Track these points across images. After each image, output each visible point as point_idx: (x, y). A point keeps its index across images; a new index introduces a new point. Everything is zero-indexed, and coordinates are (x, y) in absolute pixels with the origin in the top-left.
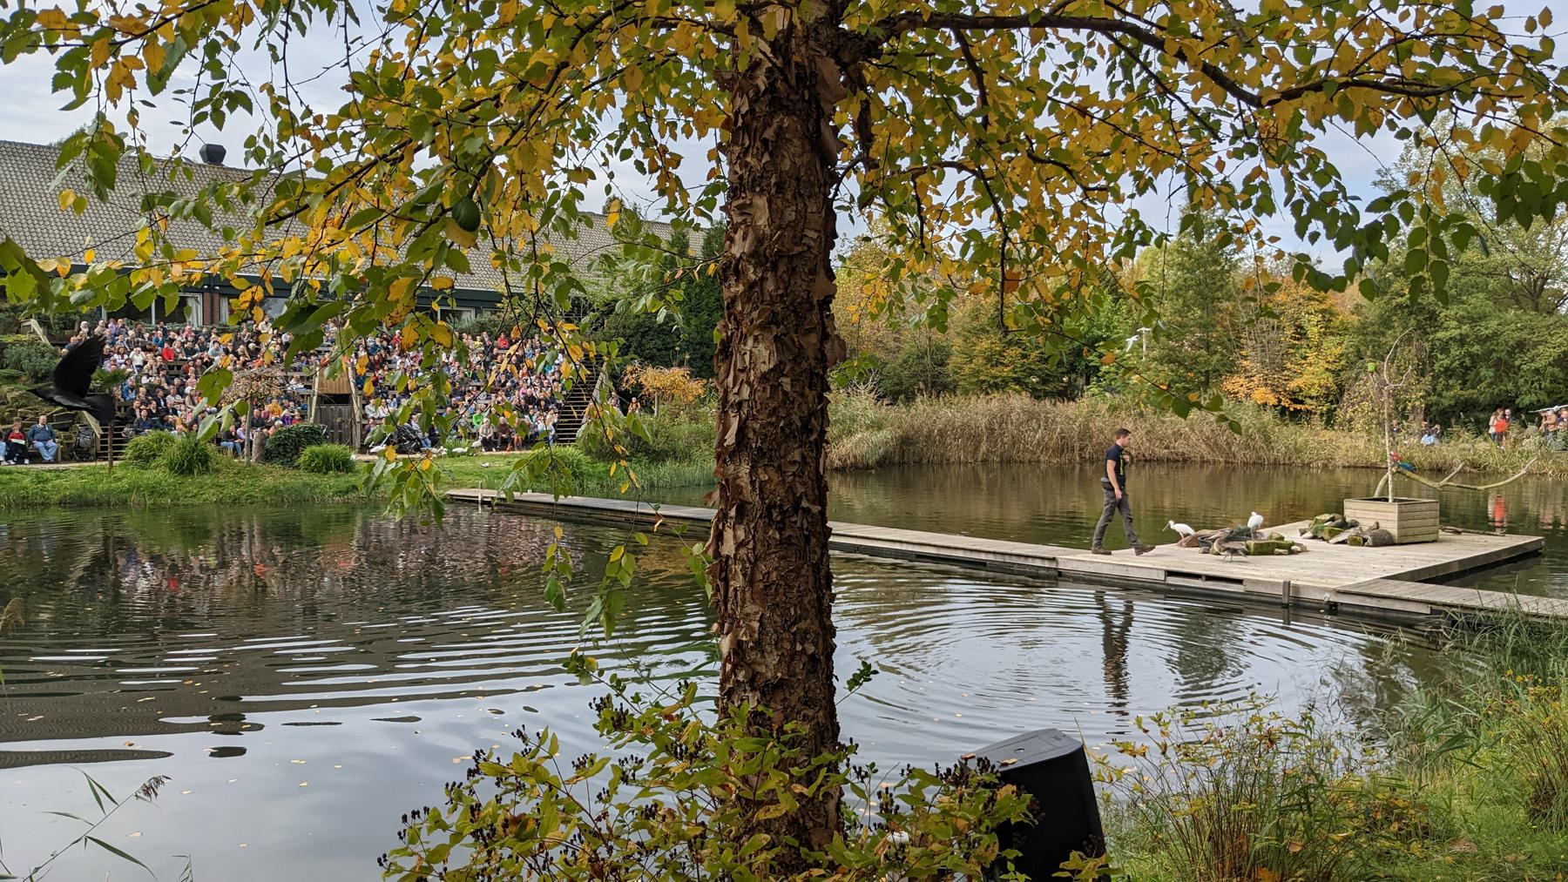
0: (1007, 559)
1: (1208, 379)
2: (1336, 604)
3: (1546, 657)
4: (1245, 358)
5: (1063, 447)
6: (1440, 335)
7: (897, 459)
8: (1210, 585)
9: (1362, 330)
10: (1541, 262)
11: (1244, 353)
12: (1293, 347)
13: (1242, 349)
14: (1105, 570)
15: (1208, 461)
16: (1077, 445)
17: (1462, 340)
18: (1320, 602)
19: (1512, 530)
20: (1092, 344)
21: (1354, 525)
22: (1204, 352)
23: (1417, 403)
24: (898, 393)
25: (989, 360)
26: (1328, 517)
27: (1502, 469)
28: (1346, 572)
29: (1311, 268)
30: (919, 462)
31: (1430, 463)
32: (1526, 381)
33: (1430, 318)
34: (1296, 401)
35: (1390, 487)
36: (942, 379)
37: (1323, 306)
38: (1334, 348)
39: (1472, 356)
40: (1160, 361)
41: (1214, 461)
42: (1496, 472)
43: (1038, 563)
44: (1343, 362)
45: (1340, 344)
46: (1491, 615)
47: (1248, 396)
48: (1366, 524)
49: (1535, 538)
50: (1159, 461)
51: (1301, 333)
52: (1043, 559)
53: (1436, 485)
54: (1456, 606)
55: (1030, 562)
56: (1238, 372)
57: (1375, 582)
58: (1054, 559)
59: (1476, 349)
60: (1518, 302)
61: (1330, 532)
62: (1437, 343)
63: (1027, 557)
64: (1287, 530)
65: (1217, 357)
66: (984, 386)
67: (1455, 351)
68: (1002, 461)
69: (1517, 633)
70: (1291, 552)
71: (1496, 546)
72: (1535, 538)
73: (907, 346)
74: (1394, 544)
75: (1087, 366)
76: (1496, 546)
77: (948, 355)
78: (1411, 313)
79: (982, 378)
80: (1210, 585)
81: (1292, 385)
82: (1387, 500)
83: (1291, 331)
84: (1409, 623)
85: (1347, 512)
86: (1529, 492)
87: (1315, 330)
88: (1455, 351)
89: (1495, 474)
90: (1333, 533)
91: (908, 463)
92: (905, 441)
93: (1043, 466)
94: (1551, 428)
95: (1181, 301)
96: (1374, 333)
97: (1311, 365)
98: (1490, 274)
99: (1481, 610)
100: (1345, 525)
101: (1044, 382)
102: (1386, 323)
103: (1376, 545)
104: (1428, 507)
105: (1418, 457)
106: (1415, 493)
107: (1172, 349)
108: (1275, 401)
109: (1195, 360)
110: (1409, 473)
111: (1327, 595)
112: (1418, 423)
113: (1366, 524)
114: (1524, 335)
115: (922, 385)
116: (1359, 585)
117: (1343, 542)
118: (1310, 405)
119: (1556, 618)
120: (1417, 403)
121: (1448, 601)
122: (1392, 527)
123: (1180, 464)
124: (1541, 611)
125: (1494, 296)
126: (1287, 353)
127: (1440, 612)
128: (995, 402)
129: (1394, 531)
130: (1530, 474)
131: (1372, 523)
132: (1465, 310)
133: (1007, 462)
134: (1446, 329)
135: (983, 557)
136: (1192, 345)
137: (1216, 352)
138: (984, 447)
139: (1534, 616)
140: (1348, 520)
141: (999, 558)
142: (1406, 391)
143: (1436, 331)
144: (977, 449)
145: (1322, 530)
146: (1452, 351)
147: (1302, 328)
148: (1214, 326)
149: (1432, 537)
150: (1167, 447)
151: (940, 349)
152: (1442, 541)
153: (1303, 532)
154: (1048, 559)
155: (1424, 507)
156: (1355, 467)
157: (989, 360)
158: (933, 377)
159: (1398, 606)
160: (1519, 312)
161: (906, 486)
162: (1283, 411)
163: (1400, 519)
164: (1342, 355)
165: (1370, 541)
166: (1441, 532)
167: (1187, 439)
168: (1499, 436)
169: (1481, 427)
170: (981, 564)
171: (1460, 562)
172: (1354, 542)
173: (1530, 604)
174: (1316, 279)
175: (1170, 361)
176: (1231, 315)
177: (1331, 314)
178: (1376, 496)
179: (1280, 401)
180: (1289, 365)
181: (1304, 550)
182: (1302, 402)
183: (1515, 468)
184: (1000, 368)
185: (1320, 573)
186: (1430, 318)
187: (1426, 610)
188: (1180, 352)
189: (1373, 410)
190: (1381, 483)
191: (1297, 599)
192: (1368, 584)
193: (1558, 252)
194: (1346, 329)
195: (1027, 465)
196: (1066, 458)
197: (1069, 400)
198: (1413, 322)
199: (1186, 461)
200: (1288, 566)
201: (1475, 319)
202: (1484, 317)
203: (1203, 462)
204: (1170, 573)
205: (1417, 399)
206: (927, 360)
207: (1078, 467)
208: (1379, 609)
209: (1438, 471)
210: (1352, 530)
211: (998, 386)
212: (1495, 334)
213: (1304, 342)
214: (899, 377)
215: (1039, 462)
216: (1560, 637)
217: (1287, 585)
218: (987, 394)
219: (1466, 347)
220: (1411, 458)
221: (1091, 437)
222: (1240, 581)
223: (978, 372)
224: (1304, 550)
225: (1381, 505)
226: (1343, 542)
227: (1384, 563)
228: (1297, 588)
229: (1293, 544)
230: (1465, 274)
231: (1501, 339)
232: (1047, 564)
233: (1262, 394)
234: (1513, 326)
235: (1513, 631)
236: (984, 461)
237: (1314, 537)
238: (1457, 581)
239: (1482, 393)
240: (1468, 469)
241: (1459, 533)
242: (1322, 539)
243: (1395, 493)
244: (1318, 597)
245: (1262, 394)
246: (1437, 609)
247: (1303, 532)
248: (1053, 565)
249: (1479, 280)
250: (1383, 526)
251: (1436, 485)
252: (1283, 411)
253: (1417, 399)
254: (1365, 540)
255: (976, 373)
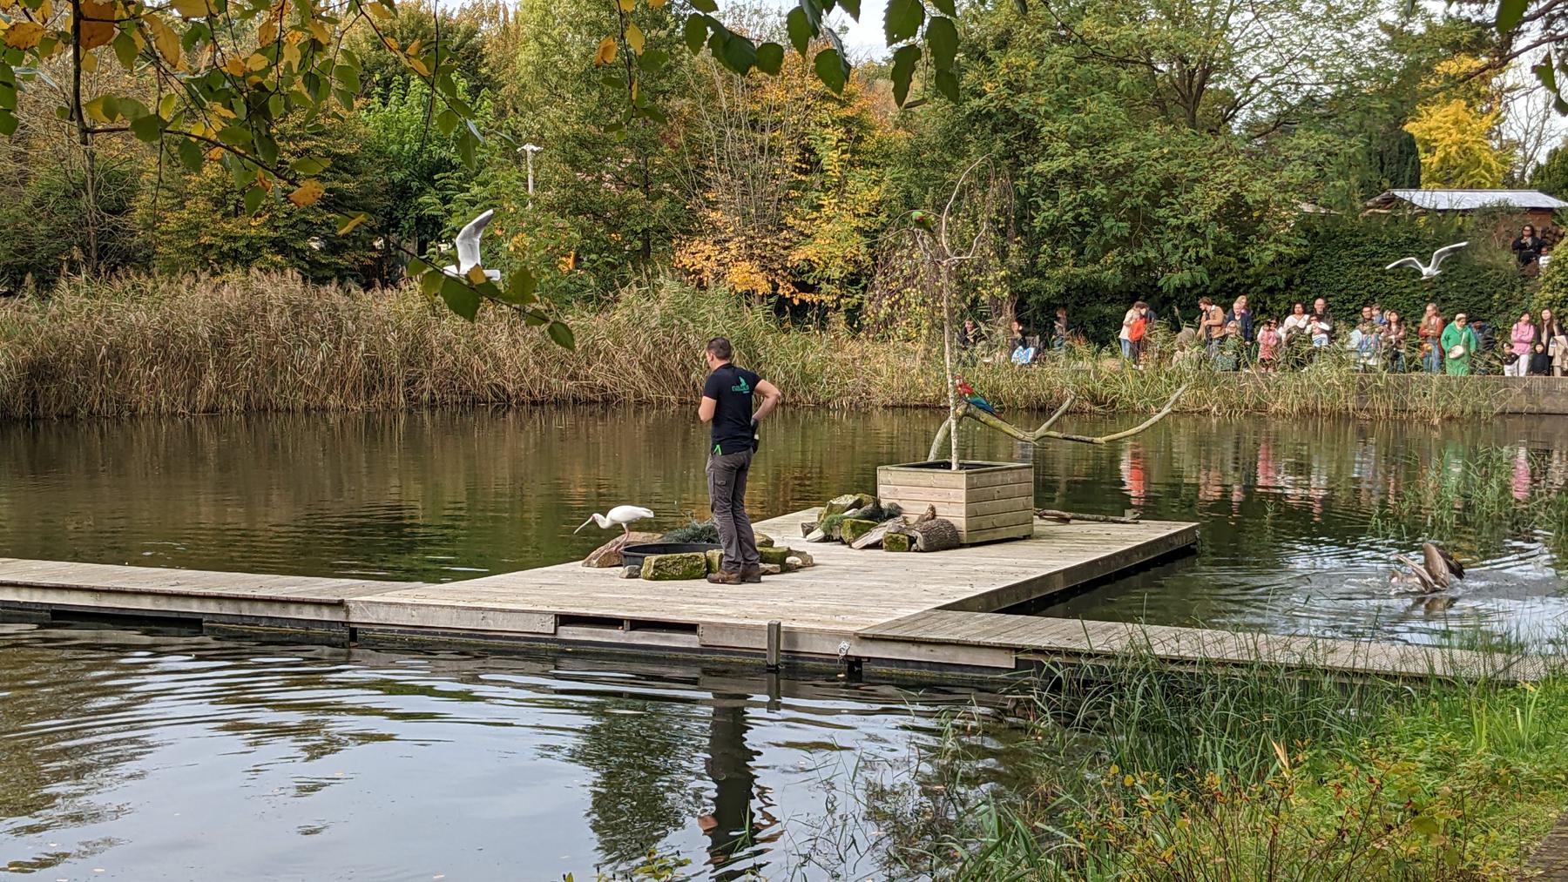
0: (246, 609)
1: (647, 243)
2: (858, 661)
3: (1192, 732)
4: (712, 205)
5: (374, 380)
6: (1041, 166)
7: (20, 410)
8: (639, 638)
9: (913, 157)
10: (1200, 43)
11: (710, 196)
12: (797, 185)
13: (708, 188)
14: (442, 620)
15: (649, 402)
16: (400, 377)
17: (1076, 178)
18: (831, 658)
19: (1151, 509)
20: (430, 172)
21: (894, 512)
22: (638, 194)
23: (997, 290)
24: (25, 270)
25: (219, 202)
26: (848, 499)
27: (1139, 406)
28: (878, 600)
29: (717, 25)
30: (70, 417)
31: (1026, 397)
32: (1176, 247)
33: (1026, 137)
34: (804, 287)
35: (954, 441)
36: (123, 241)
37: (845, 113)
38: (866, 190)
39: (1088, 201)
40: (559, 208)
41: (660, 402)
42: (1130, 410)
43: (309, 614)
44: (883, 218)
45: (876, 183)
46: (1106, 664)
47: (719, 277)
48: (914, 511)
49: (1185, 526)
50: (560, 403)
51: (809, 161)
52: (319, 604)
53: (1029, 436)
54: (1057, 652)
55: (292, 613)
56: (701, 232)
57: (926, 616)
58: (341, 604)
59: (1100, 190)
60: (1164, 110)
61: (853, 527)
62: (1038, 181)
63: (286, 602)
64: (782, 526)
65: (662, 204)
66: (212, 255)
67: (1065, 194)
68: (248, 407)
69: (1147, 694)
70: (787, 569)
71: (1124, 541)
72: (1185, 526)
73: (43, 172)
74: (962, 546)
75: (419, 219)
76: (1124, 541)
77: (133, 191)
78: (995, 130)
79: (205, 240)
80: (639, 638)
81: (797, 257)
82: (948, 466)
83: (791, 158)
84: (982, 683)
85: (882, 490)
86: (1182, 444)
87: (835, 155)
88: (1065, 194)
89: (1130, 414)
90: (859, 530)
91: (46, 418)
92: (39, 372)
93: (333, 419)
94: (1216, 333)
95: (595, 94)
96: (934, 163)
97: (829, 220)
98: (1122, 62)
99: (1089, 656)
100: (879, 515)
101: (334, 247)
102: (955, 145)
103: (931, 547)
104: (1018, 483)
105: (1007, 386)
106: (1002, 452)
107: (580, 187)
108: (767, 288)
109: (623, 209)
110: (985, 416)
111: (844, 644)
112: (1006, 326)
113: (914, 511)
114: (1174, 167)
115: (77, 254)
116: (898, 623)
117: (876, 546)
118: (827, 296)
119: (1208, 663)
120: (997, 290)
121: (1042, 643)
122: (956, 514)
123: (599, 410)
124: (1186, 653)
125: (1125, 99)
126: (787, 199)
127: (1029, 664)
128: (233, 288)
129: (960, 522)
130: (1180, 413)
131: (924, 510)
132: (1080, 122)
133: (257, 411)
134: (1052, 157)
135: (195, 607)
136: (618, 179)
137: (661, 194)
138: (210, 381)
139: (1173, 661)
140: (884, 504)
141: (228, 609)
142: (979, 270)
143: (1036, 160)
144: (194, 386)
145: (840, 525)
146: (1062, 194)
147: (812, 151)
148: (656, 145)
149: (1023, 531)
150: (573, 377)
151: (113, 178)
152: (1039, 537)
153: (808, 530)
154: (329, 604)
155: (1009, 477)
156: (904, 407)
157: (219, 202)
158: (100, 236)
159: (963, 658)
160: (1168, 128)
161: (41, 466)
162: (781, 306)
163: (969, 501)
164: (881, 203)
165: (920, 543)
166: (1037, 521)
167: (609, 360)
168: (1139, 346)
169: (1102, 335)
170: (192, 624)
171: (1066, 572)
172: (895, 544)
173: (1167, 641)
174: (727, 45)
175: (578, 211)
176: (687, 123)
177: (861, 126)
178: (931, 459)
179: (775, 287)
180: (790, 220)
181: (808, 563)
182: (812, 289)
183: (1160, 403)
184: (243, 219)
185: (833, 605)
186: (1026, 137)
187: (1007, 661)
188: (597, 193)
189: (924, 303)
190: (940, 436)
191: (793, 655)
192: (913, 620)
193: (1226, 26)
194: (887, 155)
195: (300, 415)
196: (379, 399)
197: (385, 285)
198: (999, 145)
199: (607, 402)
200: (778, 595)
201: (1096, 140)
202: (1110, 136)
203: (640, 403)
204: (565, 620)
205: (998, 283)
206: (87, 201)
207: (403, 419)
208: (932, 665)
209: (1040, 410)
210: (890, 523)
211: (241, 256)
212: (1129, 167)
213: (815, 178)
214: (27, 237)
215: (325, 409)
216: (1214, 697)
217: (775, 630)
218: (214, 274)
219: (1083, 189)
220: (995, 389)
221: (429, 359)
222: (691, 628)
223: (197, 226)
224: (808, 563)
225: (940, 476)
226: (876, 546)
227: (945, 582)
228: (792, 634)
229: (790, 552)
230: (1081, 60)
231: (1138, 176)
232: (326, 615)
233: (745, 274)
234: (1156, 153)
235: (1140, 690)
236: (212, 411)
237: (827, 539)
238: (1060, 607)
239: (1109, 270)
240: (1087, 406)
241: (1066, 521)
242: (841, 541)
243: (962, 456)
244: (829, 648)
245: (745, 274)
246: (1029, 659)
247: (808, 530)
248: (340, 616)
249: (1103, 71)
250: (942, 513)
251: (1029, 436)
252: (781, 306)
253: (998, 283)
254: (912, 540)
255: (194, 228)
